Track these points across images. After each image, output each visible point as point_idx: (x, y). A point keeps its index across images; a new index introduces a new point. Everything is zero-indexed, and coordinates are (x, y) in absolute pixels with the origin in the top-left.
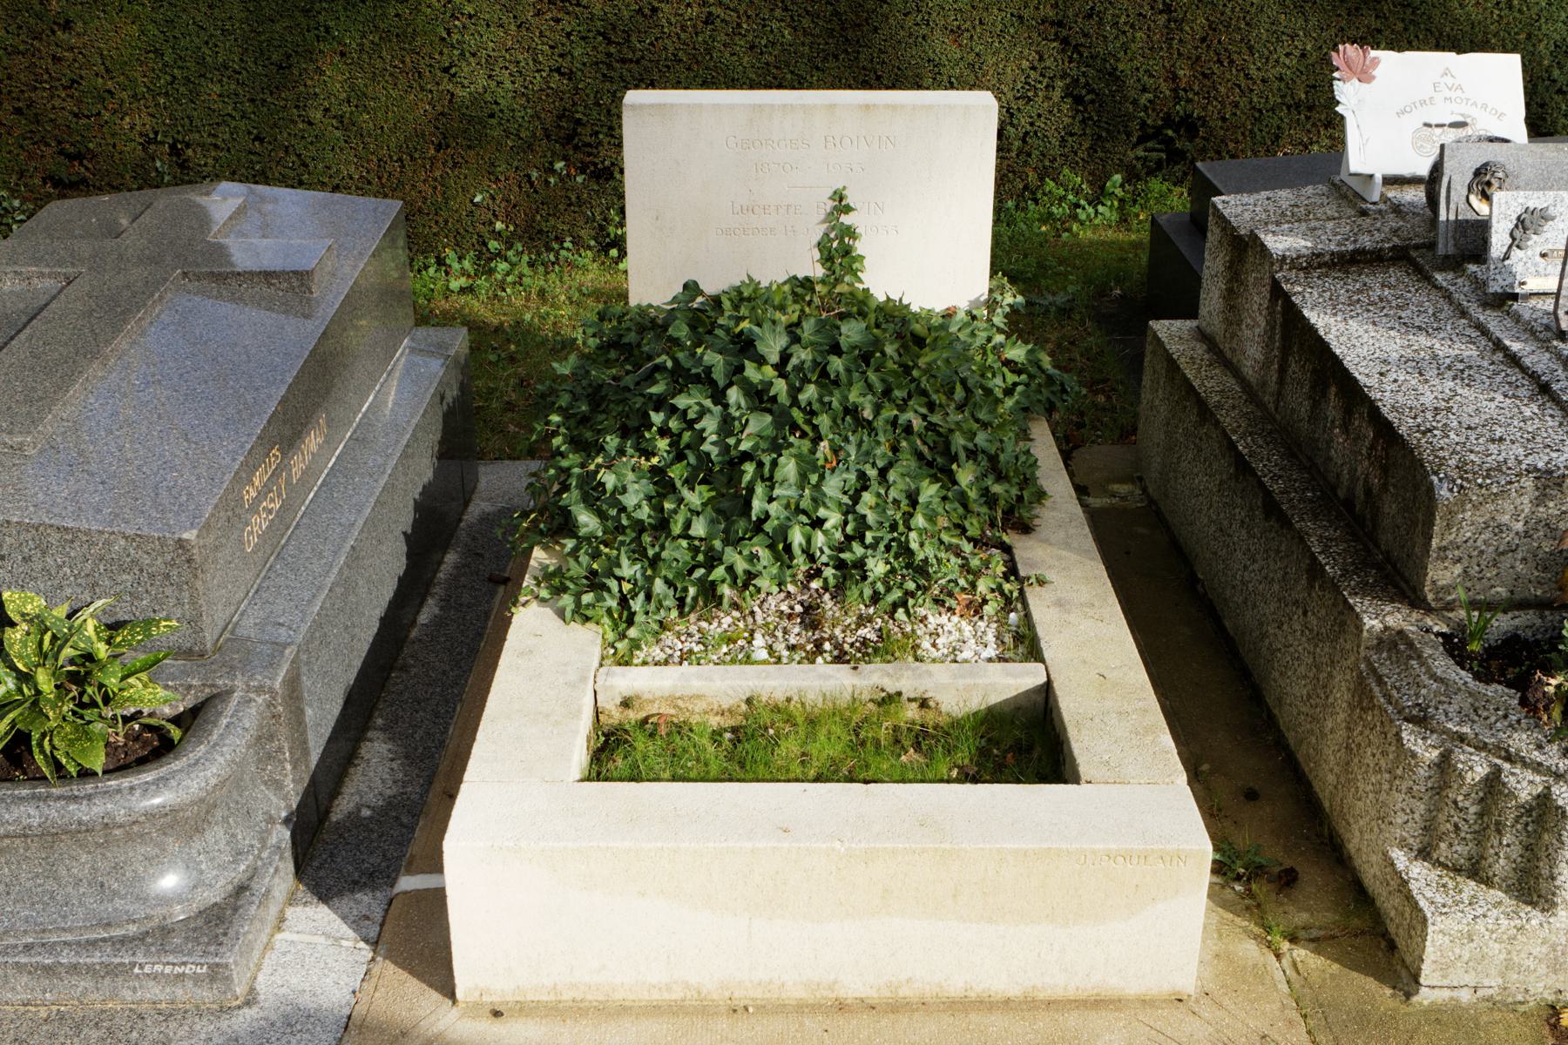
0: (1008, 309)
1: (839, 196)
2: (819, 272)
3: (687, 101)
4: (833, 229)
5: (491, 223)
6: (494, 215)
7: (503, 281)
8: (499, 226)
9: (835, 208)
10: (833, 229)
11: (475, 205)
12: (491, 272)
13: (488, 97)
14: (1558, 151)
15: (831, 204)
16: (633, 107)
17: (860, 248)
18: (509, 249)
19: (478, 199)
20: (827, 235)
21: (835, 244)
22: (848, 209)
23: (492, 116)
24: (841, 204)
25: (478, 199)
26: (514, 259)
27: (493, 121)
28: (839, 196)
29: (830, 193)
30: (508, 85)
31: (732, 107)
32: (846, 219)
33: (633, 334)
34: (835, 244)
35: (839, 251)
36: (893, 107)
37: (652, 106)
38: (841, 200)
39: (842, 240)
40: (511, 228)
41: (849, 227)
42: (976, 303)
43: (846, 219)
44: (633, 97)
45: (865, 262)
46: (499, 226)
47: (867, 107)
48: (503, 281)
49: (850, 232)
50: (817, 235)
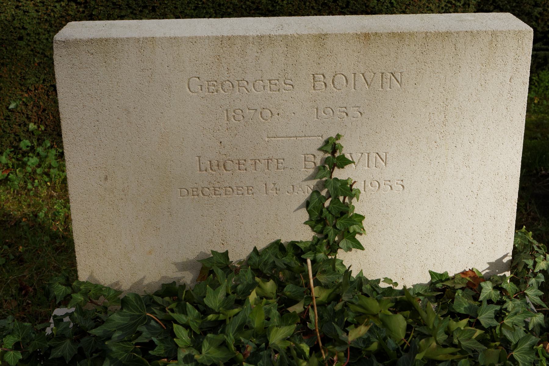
0: (542, 279)
1: (331, 147)
2: (305, 235)
3: (135, 34)
4: (324, 185)
5: (25, 125)
6: (28, 118)
7: (34, 172)
8: (32, 126)
9: (326, 161)
10: (324, 185)
11: (11, 111)
12: (24, 165)
13: (16, 24)
14: (475, 16)
15: (321, 156)
16: (66, 43)
17: (359, 207)
18: (39, 145)
19: (12, 106)
20: (316, 192)
21: (327, 204)
22: (343, 162)
23: (21, 38)
24: (333, 155)
25: (12, 106)
26: (43, 154)
27: (21, 43)
28: (331, 147)
29: (320, 142)
30: (34, 14)
31: (194, 40)
32: (339, 174)
33: (67, 343)
34: (327, 204)
35: (334, 214)
36: (399, 36)
37: (91, 41)
38: (334, 151)
39: (336, 198)
40: (43, 128)
41: (344, 183)
42: (497, 265)
43: (339, 174)
44: (75, 30)
45: (365, 223)
46: (32, 126)
47: (367, 36)
48: (34, 172)
49: (347, 189)
50: (305, 191)
